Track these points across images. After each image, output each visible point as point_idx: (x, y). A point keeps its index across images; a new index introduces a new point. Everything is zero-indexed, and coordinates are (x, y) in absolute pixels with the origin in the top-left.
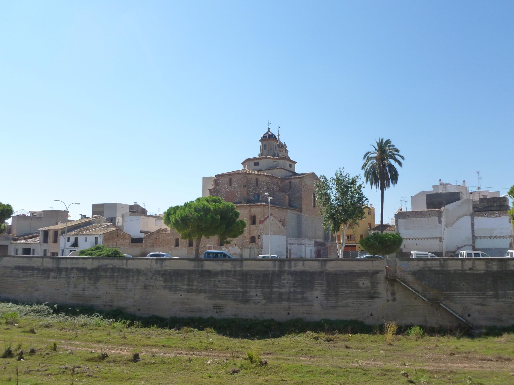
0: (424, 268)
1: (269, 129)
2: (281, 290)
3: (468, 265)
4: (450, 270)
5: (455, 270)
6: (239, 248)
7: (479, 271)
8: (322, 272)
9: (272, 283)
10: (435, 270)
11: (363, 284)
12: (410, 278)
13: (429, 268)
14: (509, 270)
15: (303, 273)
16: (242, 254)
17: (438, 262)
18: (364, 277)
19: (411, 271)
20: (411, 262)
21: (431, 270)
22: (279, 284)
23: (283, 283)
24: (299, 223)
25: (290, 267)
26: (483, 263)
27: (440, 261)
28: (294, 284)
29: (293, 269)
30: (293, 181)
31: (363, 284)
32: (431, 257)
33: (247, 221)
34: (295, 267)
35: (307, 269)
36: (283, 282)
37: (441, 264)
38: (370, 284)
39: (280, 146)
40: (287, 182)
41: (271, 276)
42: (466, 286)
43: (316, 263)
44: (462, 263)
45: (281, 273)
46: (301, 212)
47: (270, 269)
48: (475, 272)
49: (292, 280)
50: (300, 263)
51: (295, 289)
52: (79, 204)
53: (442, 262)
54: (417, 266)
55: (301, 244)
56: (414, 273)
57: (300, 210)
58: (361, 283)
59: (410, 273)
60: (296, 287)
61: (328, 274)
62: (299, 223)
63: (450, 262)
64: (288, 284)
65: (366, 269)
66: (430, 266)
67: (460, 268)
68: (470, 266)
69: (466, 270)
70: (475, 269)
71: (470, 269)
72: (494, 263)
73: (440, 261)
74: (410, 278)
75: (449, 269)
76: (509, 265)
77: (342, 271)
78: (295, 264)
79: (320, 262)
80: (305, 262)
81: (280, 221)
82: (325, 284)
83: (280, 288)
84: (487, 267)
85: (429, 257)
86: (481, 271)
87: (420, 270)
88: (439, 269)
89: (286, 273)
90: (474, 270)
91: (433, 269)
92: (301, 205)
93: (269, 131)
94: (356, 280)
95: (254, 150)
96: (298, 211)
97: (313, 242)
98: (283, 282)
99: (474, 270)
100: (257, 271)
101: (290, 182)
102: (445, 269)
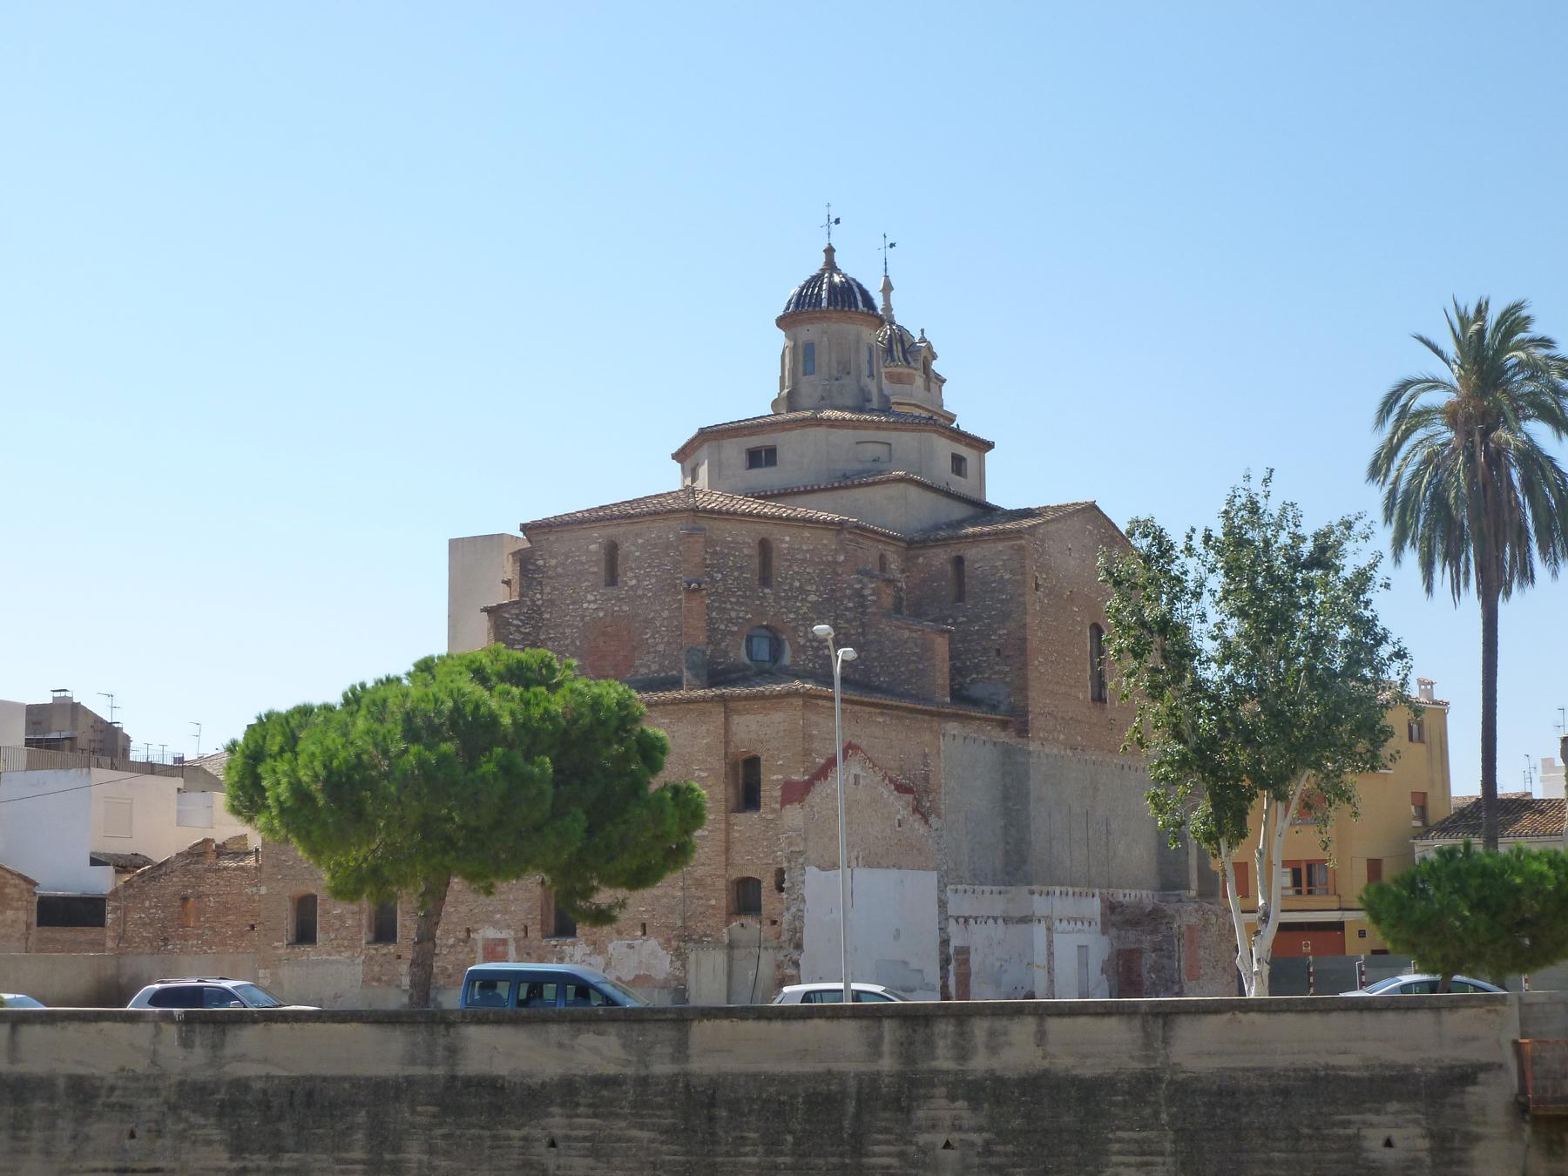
1: (830, 251)
6: (666, 944)
8: (1147, 1082)
11: (1388, 1143)
15: (1037, 1085)
18: (1394, 1106)
23: (924, 1151)
24: (1013, 797)
25: (963, 1054)
29: (980, 1063)
30: (971, 553)
31: (1388, 1143)
33: (711, 791)
34: (993, 1049)
35: (1064, 1062)
36: (923, 1138)
38: (1424, 1144)
39: (898, 351)
40: (940, 558)
41: (851, 1107)
46: (1023, 731)
49: (980, 1129)
50: (1022, 1031)
55: (1025, 920)
57: (1017, 721)
58: (1373, 1141)
61: (1183, 1089)
62: (1013, 797)
65: (1402, 1058)
77: (1265, 1073)
78: (992, 1034)
79: (1137, 1022)
80: (1053, 1024)
81: (901, 789)
82: (1168, 1146)
89: (941, 1091)
92: (1023, 690)
93: (830, 266)
94: (1346, 1124)
96: (1004, 725)
97: (1094, 907)
98: (923, 1138)
100: (771, 1079)
101: (959, 562)
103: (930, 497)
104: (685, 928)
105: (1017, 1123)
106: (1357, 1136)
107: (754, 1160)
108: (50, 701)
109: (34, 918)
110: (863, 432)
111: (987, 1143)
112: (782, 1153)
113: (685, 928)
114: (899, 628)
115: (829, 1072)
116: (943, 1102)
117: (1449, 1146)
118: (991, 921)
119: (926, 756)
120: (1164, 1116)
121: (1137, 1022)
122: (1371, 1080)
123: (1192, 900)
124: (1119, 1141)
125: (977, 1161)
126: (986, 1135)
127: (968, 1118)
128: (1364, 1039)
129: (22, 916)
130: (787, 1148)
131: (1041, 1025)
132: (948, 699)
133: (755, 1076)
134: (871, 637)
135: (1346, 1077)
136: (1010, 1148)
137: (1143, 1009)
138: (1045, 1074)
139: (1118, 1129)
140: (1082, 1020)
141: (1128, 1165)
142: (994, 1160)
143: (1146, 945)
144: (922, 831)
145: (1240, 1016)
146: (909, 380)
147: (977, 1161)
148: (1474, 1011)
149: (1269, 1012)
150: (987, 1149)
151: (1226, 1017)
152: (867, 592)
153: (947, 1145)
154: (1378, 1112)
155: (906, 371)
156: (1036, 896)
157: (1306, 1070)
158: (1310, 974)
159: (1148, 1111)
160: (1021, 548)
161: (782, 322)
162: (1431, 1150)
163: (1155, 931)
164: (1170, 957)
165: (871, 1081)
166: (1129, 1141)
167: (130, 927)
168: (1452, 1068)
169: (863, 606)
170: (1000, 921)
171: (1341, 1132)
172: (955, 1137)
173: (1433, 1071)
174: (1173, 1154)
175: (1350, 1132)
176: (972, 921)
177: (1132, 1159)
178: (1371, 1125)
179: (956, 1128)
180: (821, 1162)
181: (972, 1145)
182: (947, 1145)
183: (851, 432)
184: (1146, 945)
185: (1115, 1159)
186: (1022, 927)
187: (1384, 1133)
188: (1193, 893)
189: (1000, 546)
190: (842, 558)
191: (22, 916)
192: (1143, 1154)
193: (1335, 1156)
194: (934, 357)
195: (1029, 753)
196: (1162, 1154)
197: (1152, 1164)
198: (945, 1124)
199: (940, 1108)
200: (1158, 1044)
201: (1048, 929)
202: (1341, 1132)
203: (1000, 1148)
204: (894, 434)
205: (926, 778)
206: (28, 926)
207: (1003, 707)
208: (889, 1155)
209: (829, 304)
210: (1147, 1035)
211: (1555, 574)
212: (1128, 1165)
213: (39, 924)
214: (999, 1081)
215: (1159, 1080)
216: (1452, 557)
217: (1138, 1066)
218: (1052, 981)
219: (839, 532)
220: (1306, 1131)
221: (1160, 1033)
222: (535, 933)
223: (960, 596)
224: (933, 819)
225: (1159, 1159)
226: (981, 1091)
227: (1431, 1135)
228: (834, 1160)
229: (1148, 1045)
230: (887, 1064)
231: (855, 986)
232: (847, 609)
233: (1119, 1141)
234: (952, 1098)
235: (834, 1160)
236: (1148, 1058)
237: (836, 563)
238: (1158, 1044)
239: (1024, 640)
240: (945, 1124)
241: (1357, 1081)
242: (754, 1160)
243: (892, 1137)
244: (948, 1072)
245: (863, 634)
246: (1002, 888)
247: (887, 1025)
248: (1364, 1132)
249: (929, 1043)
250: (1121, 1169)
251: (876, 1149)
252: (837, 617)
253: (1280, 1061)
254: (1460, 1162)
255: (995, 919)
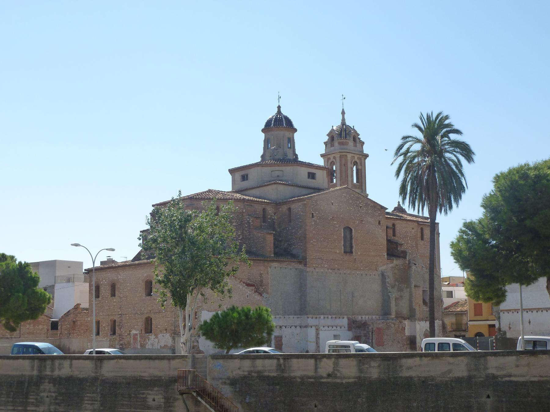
0: (250, 372)
1: (279, 107)
2: (38, 409)
3: (326, 367)
4: (295, 378)
5: (302, 378)
6: (171, 336)
7: (345, 378)
8: (95, 379)
9: (27, 398)
10: (268, 377)
11: (154, 400)
12: (227, 391)
13: (259, 372)
14: (401, 377)
15: (70, 379)
16: (174, 347)
17: (275, 362)
18: (156, 389)
19: (228, 378)
20: (230, 361)
21: (262, 377)
22: (36, 399)
23: (41, 398)
24: (301, 287)
25: (53, 370)
26: (353, 362)
27: (278, 359)
28: (56, 399)
29: (57, 373)
30: (293, 206)
31: (154, 400)
32: (356, 351)
33: (158, 289)
34: (60, 369)
35: (76, 373)
36: (42, 394)
37: (279, 365)
38: (163, 400)
39: (343, 134)
40: (285, 208)
41: (26, 385)
42: (320, 407)
43: (27, 363)
44: (316, 365)
45: (41, 379)
46: (305, 265)
47: (27, 373)
48: (338, 381)
49: (54, 392)
50: (67, 363)
51: (57, 407)
52: (349, 251)
53: (282, 361)
54: (239, 369)
55: (306, 327)
56: (233, 382)
57: (303, 261)
58: (150, 399)
59: (228, 382)
60: (58, 404)
61: (104, 382)
62: (301, 287)
63: (295, 361)
64: (48, 399)
65: (159, 374)
66: (260, 368)
67: (311, 373)
68: (330, 370)
69: (322, 377)
70: (338, 374)
71: (329, 375)
72: (373, 364)
73: (278, 359)
74: (227, 391)
75: (292, 375)
76: (401, 366)
77: (124, 378)
78: (60, 364)
79: (94, 362)
80: (74, 362)
81: (248, 285)
82: (99, 399)
83: (37, 406)
84: (361, 371)
85: (353, 352)
86: (349, 378)
87: (245, 377)
88: (275, 374)
89: (47, 381)
90: (336, 377)
91: (266, 374)
92: (305, 251)
93: (279, 112)
94: (143, 394)
95: (252, 151)
96: (300, 263)
97: (345, 322)
98: (42, 394)
99: (336, 377)
100: (10, 376)
101: (290, 209)
102: (286, 375)
103: (290, 187)
104: (175, 330)
105: (63, 391)
106: (146, 398)
107: (3, 399)
108: (106, 260)
109: (50, 328)
110: (272, 168)
111: (56, 396)
112: (10, 398)
113: (175, 330)
114: (258, 233)
115: (22, 375)
116: (47, 384)
117: (169, 402)
118: (293, 327)
119: (261, 274)
120: (99, 390)
121: (94, 362)
122: (151, 380)
123: (393, 319)
124: (87, 397)
125: (53, 401)
126: (56, 394)
127: (53, 389)
128: (150, 368)
129: (45, 327)
130: (11, 396)
131: (71, 362)
132: (273, 255)
133: (6, 375)
134: (252, 236)
135: (144, 380)
136: (61, 398)
137: (95, 358)
138: (71, 377)
139: (87, 393)
140: (81, 361)
141: (89, 404)
142: (57, 401)
143: (362, 335)
144: (258, 298)
145: (119, 360)
146: (347, 144)
147: (53, 401)
148: (180, 360)
149: (126, 359)
150: (56, 399)
151: (116, 361)
152: (250, 221)
153: (47, 397)
154: (152, 391)
155: (345, 141)
156: (310, 319)
157: (135, 377)
158: (477, 343)
159: (95, 388)
160: (305, 204)
161: (263, 131)
162: (164, 402)
163: (365, 330)
164: (368, 338)
165: (31, 377)
166: (90, 397)
167: (63, 330)
168: (173, 377)
169: (250, 226)
170: (298, 327)
171: (142, 396)
172: (50, 394)
173: (167, 378)
174: (100, 401)
175: (144, 396)
176: (284, 327)
177: (90, 402)
178: (150, 394)
179: (50, 392)
180: (18, 400)
181: (52, 396)
182: (47, 397)
183: (269, 168)
184: (362, 335)
185: (86, 402)
186: (305, 329)
187: (153, 397)
188: (393, 316)
189: (300, 204)
190: (244, 211)
191: (45, 327)
192: (92, 401)
193: (140, 403)
194: (358, 135)
195: (307, 272)
196: (97, 401)
197: (95, 404)
198: (48, 390)
199: (47, 386)
200: (99, 368)
201: (317, 329)
202: (142, 396)
203: (59, 398)
204: (284, 167)
205: (261, 281)
206: (48, 330)
207: (301, 257)
208: (33, 399)
209: (274, 125)
210: (96, 365)
211: (458, 206)
212: (89, 404)
213: (52, 329)
214: (61, 378)
215: (98, 379)
216: (421, 200)
217: (93, 375)
218: (319, 347)
219: (244, 202)
220: (133, 395)
221: (99, 365)
222: (143, 332)
223: (290, 221)
224: (264, 295)
225: (96, 403)
226: (56, 381)
227: (165, 398)
228: (21, 400)
229: (96, 368)
230: (35, 373)
231: (96, 350)
232: (246, 227)
233: (87, 397)
234: (49, 383)
235: (21, 400)
236: (96, 373)
237: (243, 212)
238: (99, 368)
239: (306, 234)
240: (48, 390)
241: (147, 381)
242: (3, 399)
243: (34, 394)
244: (49, 375)
245: (249, 235)
246: (299, 316)
247: (36, 361)
248: (148, 396)
249: (45, 367)
250: (87, 405)
251: (31, 397)
252: (243, 230)
253: (128, 374)
254: (172, 406)
255: (296, 327)
